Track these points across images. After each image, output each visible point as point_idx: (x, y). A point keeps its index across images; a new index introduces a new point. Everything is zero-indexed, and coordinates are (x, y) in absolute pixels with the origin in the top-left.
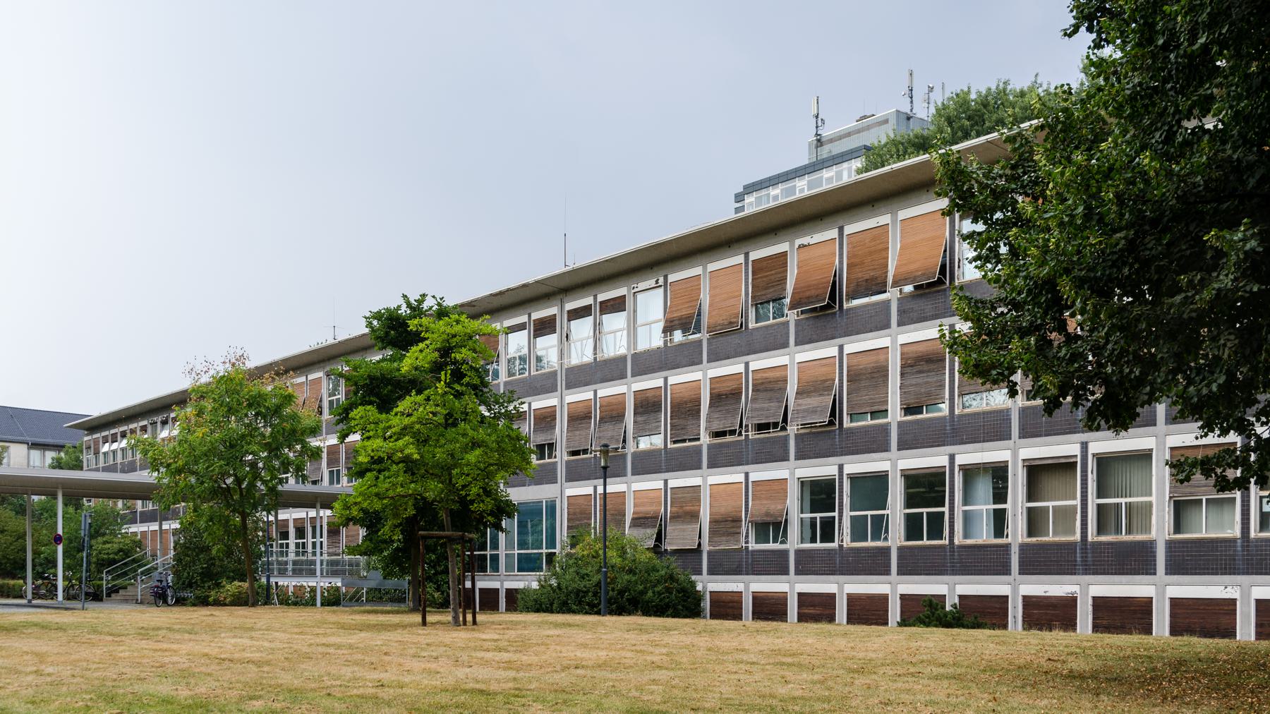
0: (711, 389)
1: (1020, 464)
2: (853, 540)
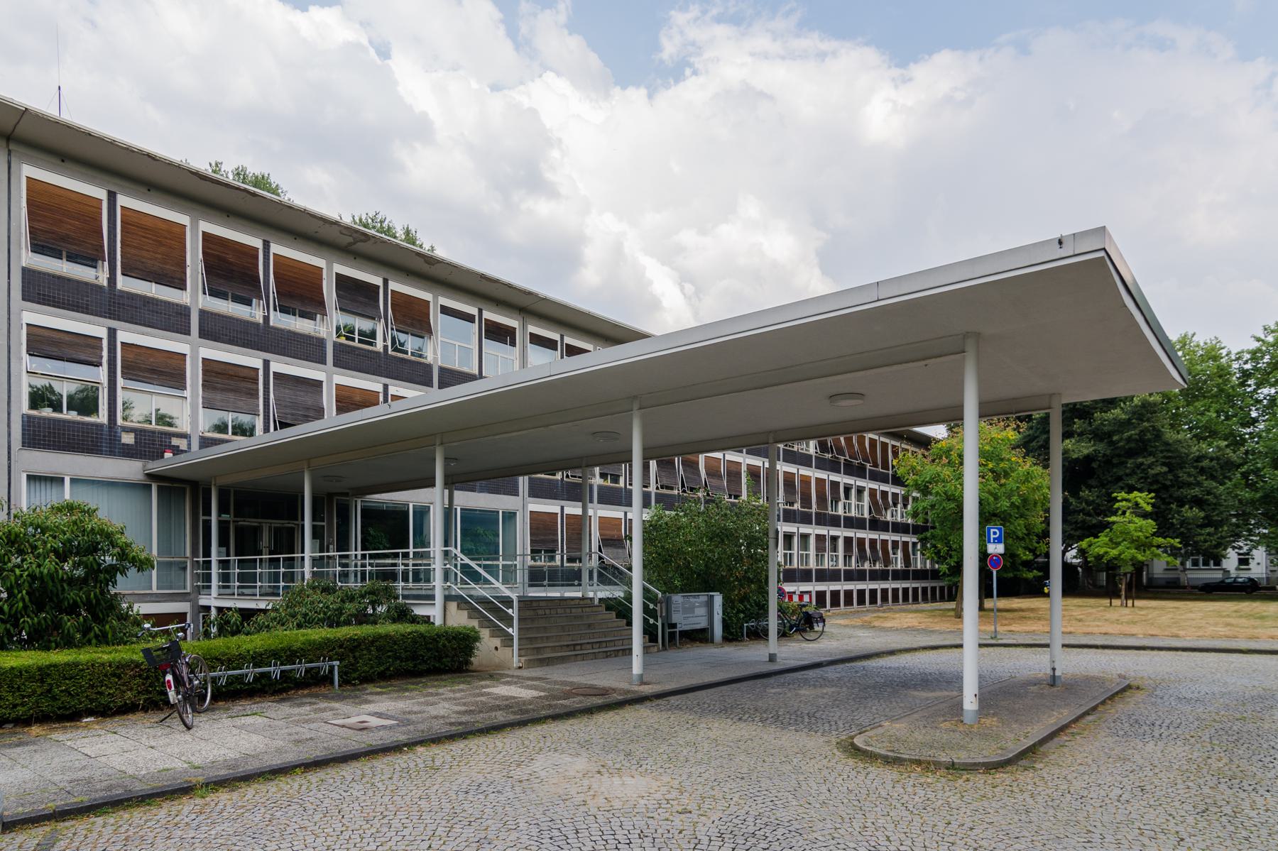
0: (337, 395)
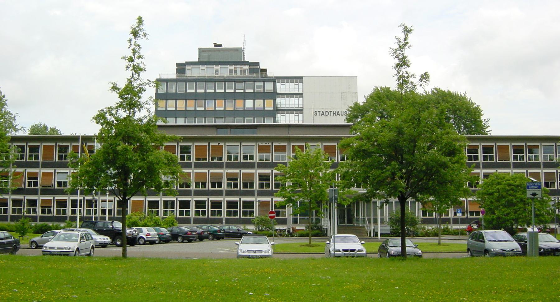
1: (11, 200)
2: (180, 215)
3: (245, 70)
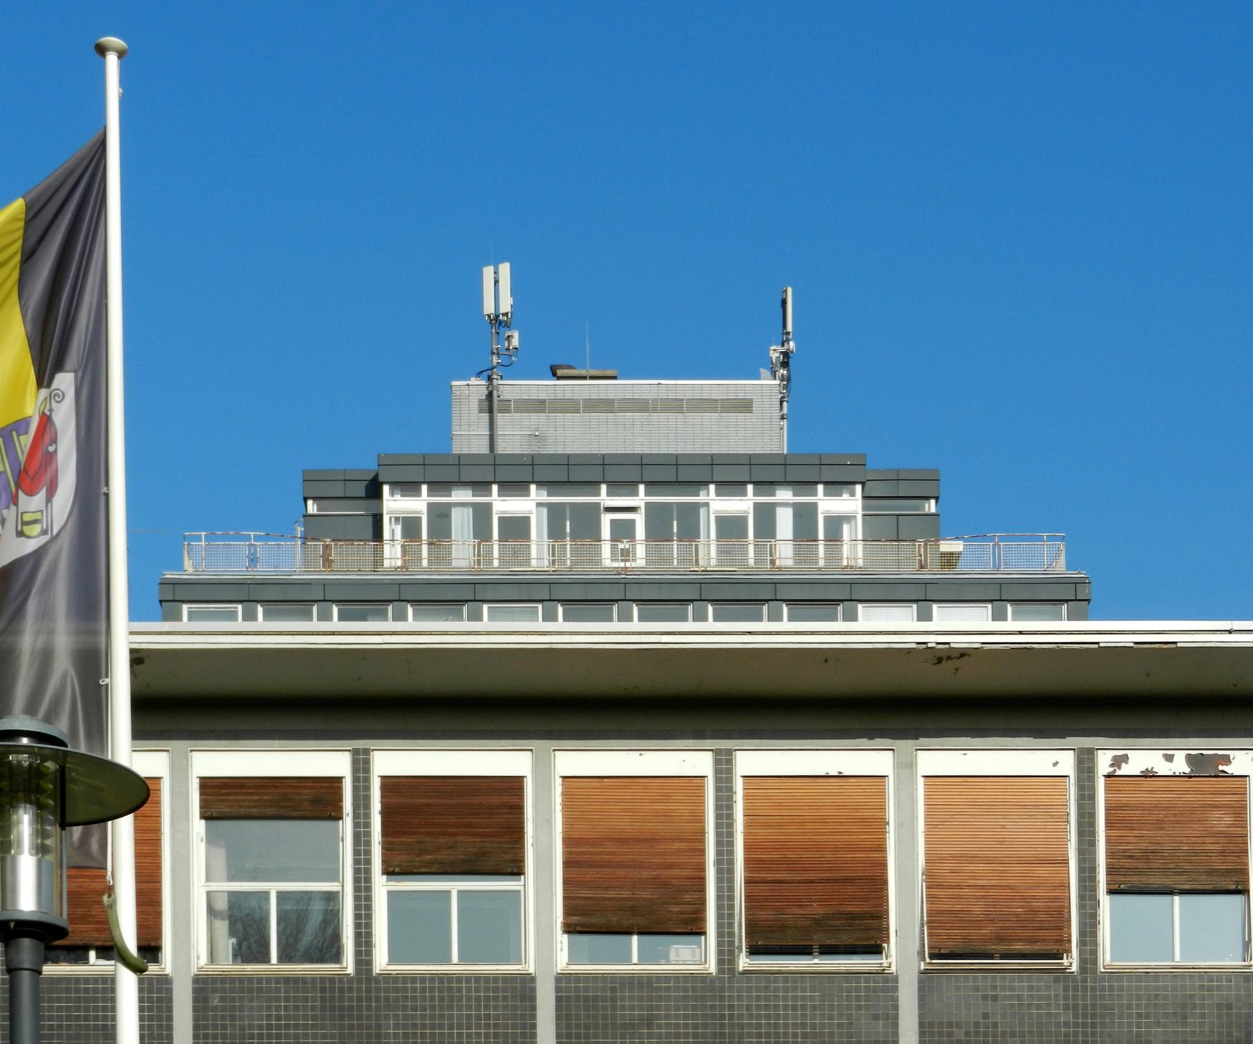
3: (835, 523)
